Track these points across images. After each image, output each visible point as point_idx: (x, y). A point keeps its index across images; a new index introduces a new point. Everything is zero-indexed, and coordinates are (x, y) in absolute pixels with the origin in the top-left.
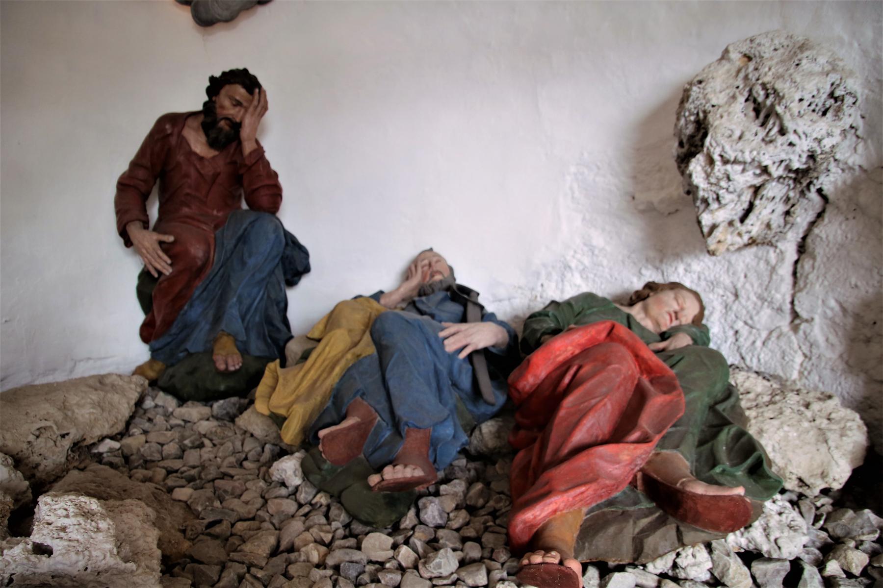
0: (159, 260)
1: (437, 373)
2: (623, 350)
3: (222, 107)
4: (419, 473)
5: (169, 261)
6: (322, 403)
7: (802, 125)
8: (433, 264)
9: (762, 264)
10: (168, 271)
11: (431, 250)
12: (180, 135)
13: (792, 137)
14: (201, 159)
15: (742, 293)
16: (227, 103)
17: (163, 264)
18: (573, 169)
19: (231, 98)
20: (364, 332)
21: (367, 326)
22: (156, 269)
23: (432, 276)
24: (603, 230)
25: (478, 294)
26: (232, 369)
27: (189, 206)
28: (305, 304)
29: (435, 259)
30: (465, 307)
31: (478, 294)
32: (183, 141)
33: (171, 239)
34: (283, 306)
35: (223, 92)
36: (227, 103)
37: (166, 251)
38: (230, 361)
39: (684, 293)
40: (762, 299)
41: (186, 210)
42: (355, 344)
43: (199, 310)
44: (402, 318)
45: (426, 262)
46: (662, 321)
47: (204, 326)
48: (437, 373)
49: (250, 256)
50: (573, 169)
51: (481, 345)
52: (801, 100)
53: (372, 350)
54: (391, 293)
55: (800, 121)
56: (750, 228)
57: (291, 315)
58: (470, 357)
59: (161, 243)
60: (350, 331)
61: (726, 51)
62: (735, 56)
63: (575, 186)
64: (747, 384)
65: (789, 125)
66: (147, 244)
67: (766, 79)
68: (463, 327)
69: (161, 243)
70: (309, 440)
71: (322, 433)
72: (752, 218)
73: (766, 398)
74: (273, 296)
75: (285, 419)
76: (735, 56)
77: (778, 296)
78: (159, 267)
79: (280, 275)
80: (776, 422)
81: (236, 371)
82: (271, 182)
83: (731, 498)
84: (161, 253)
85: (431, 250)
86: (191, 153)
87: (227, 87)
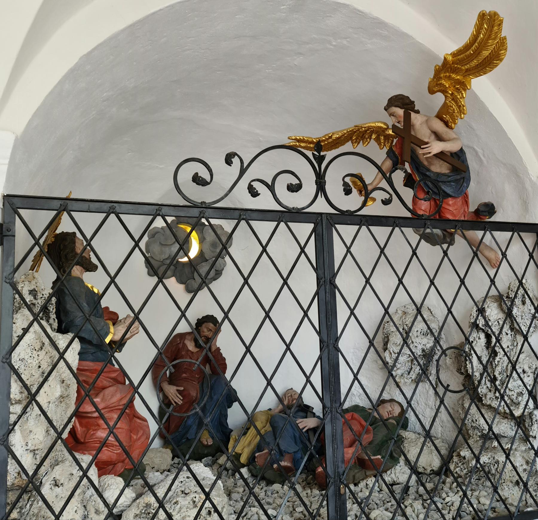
0: (177, 398)
1: (295, 436)
2: (356, 422)
3: (203, 332)
4: (289, 465)
5: (182, 398)
6: (254, 448)
7: (418, 340)
8: (293, 395)
9: (425, 390)
10: (180, 402)
11: (292, 389)
12: (183, 343)
13: (415, 344)
14: (192, 353)
15: (419, 403)
16: (205, 330)
17: (179, 399)
18: (352, 351)
19: (207, 328)
20: (267, 423)
21: (267, 421)
22: (175, 402)
23: (293, 401)
24: (366, 377)
25: (313, 408)
26: (209, 444)
27: (186, 374)
28: (235, 416)
29: (294, 393)
30: (307, 413)
31: (313, 408)
32: (185, 345)
33: (182, 388)
34: (226, 416)
35: (204, 325)
36: (205, 330)
37: (180, 394)
38: (208, 440)
39: (395, 403)
40: (426, 404)
41: (184, 375)
42: (264, 427)
43: (192, 420)
44: (281, 416)
45: (290, 394)
46: (384, 415)
47: (195, 427)
48: (295, 436)
49: (214, 395)
50: (352, 351)
51: (312, 427)
52: (417, 331)
53: (270, 429)
54: (275, 409)
55: (417, 339)
56: (411, 376)
57: (229, 421)
58: (307, 431)
59: (177, 390)
60: (262, 422)
61: (397, 310)
62: (400, 312)
63: (354, 358)
64: (409, 436)
65: (414, 340)
66: (172, 391)
67: (407, 323)
68: (305, 419)
69: (177, 390)
70: (252, 460)
71: (257, 455)
72: (412, 372)
73: (414, 440)
74: (223, 413)
75: (241, 454)
76: (400, 312)
77: (431, 403)
78: (177, 401)
79: (226, 404)
80: (414, 448)
81: (211, 445)
82: (222, 362)
83: (376, 459)
84: (178, 395)
85: (292, 389)
86: (188, 350)
87: (206, 324)
